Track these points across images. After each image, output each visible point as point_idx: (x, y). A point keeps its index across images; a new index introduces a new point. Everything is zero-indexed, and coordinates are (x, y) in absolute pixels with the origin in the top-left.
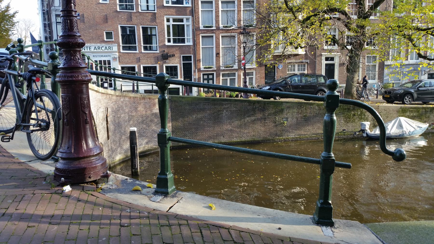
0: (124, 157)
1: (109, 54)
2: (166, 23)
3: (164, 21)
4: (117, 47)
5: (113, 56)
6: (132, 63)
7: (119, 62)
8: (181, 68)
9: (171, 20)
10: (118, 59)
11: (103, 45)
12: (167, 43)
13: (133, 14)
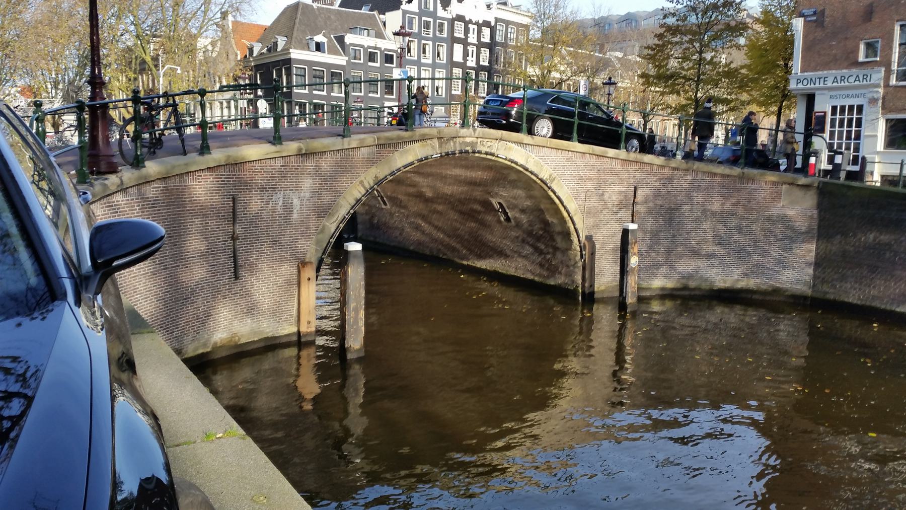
0: (679, 285)
1: (863, 91)
5: (870, 95)
10: (880, 102)
11: (854, 71)
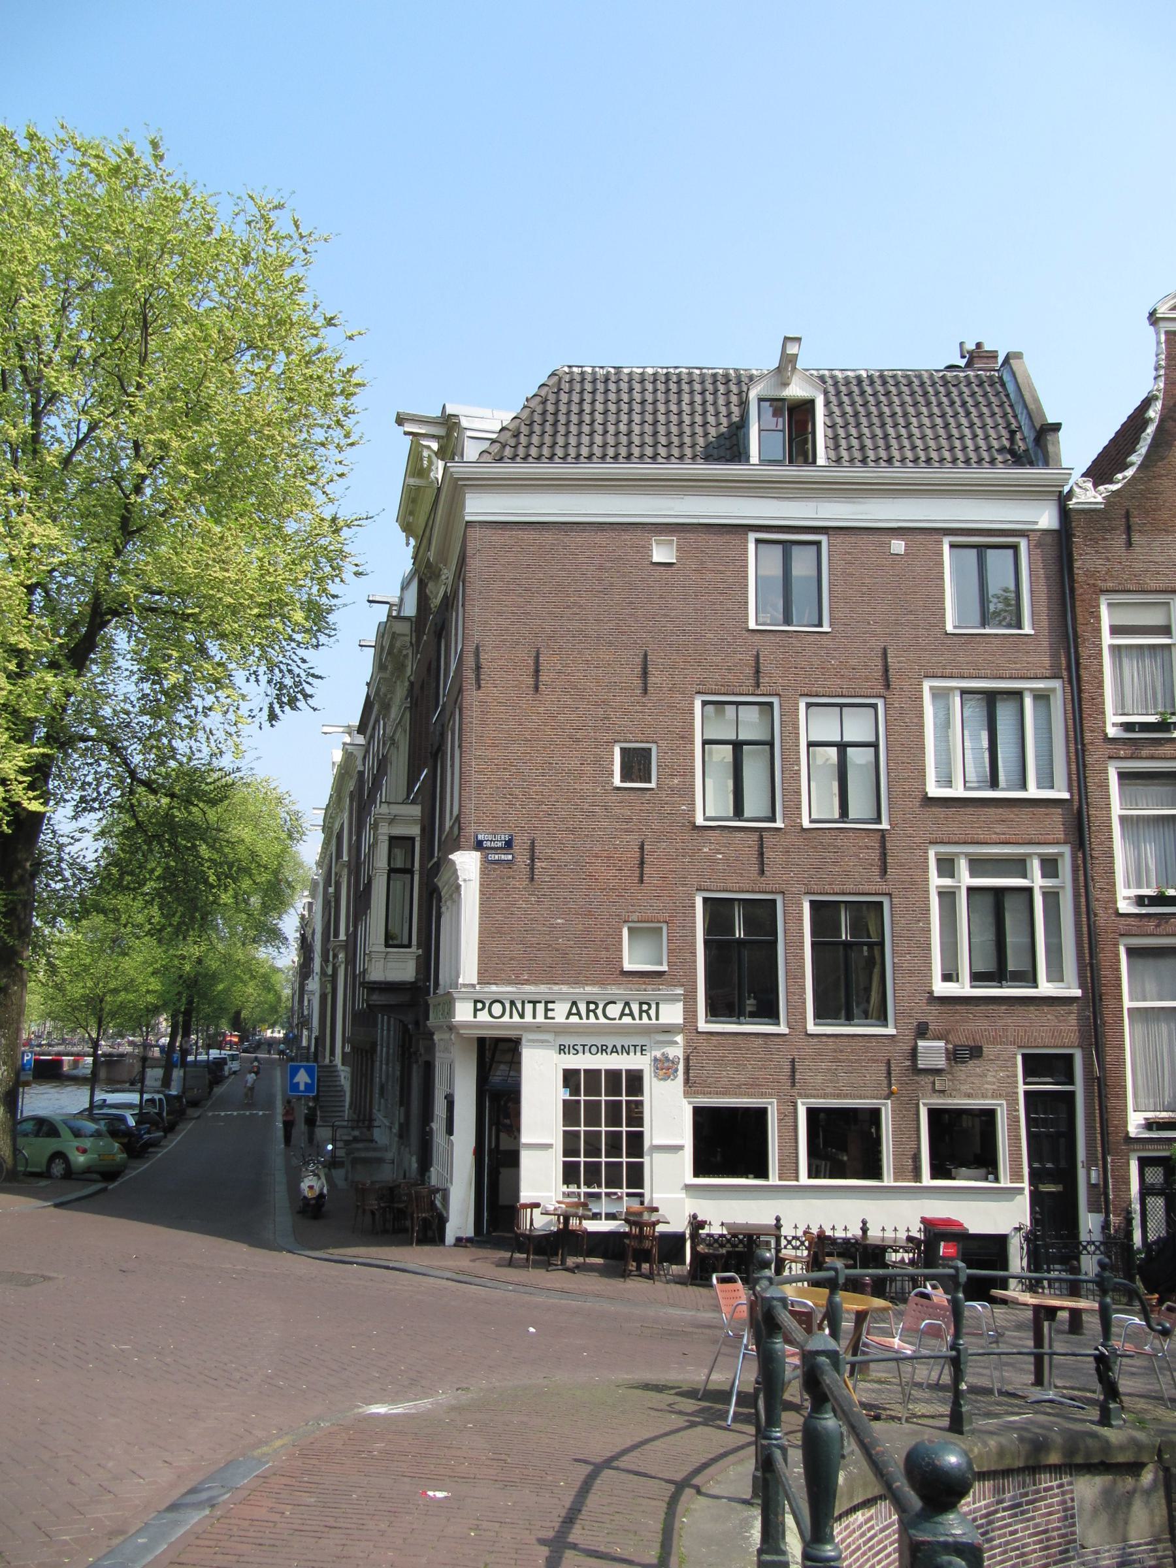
2: (936, 881)
3: (926, 869)
4: (680, 1006)
6: (753, 1087)
7: (687, 1081)
8: (1014, 1120)
9: (963, 866)
10: (681, 1067)
12: (941, 988)
13: (769, 840)
